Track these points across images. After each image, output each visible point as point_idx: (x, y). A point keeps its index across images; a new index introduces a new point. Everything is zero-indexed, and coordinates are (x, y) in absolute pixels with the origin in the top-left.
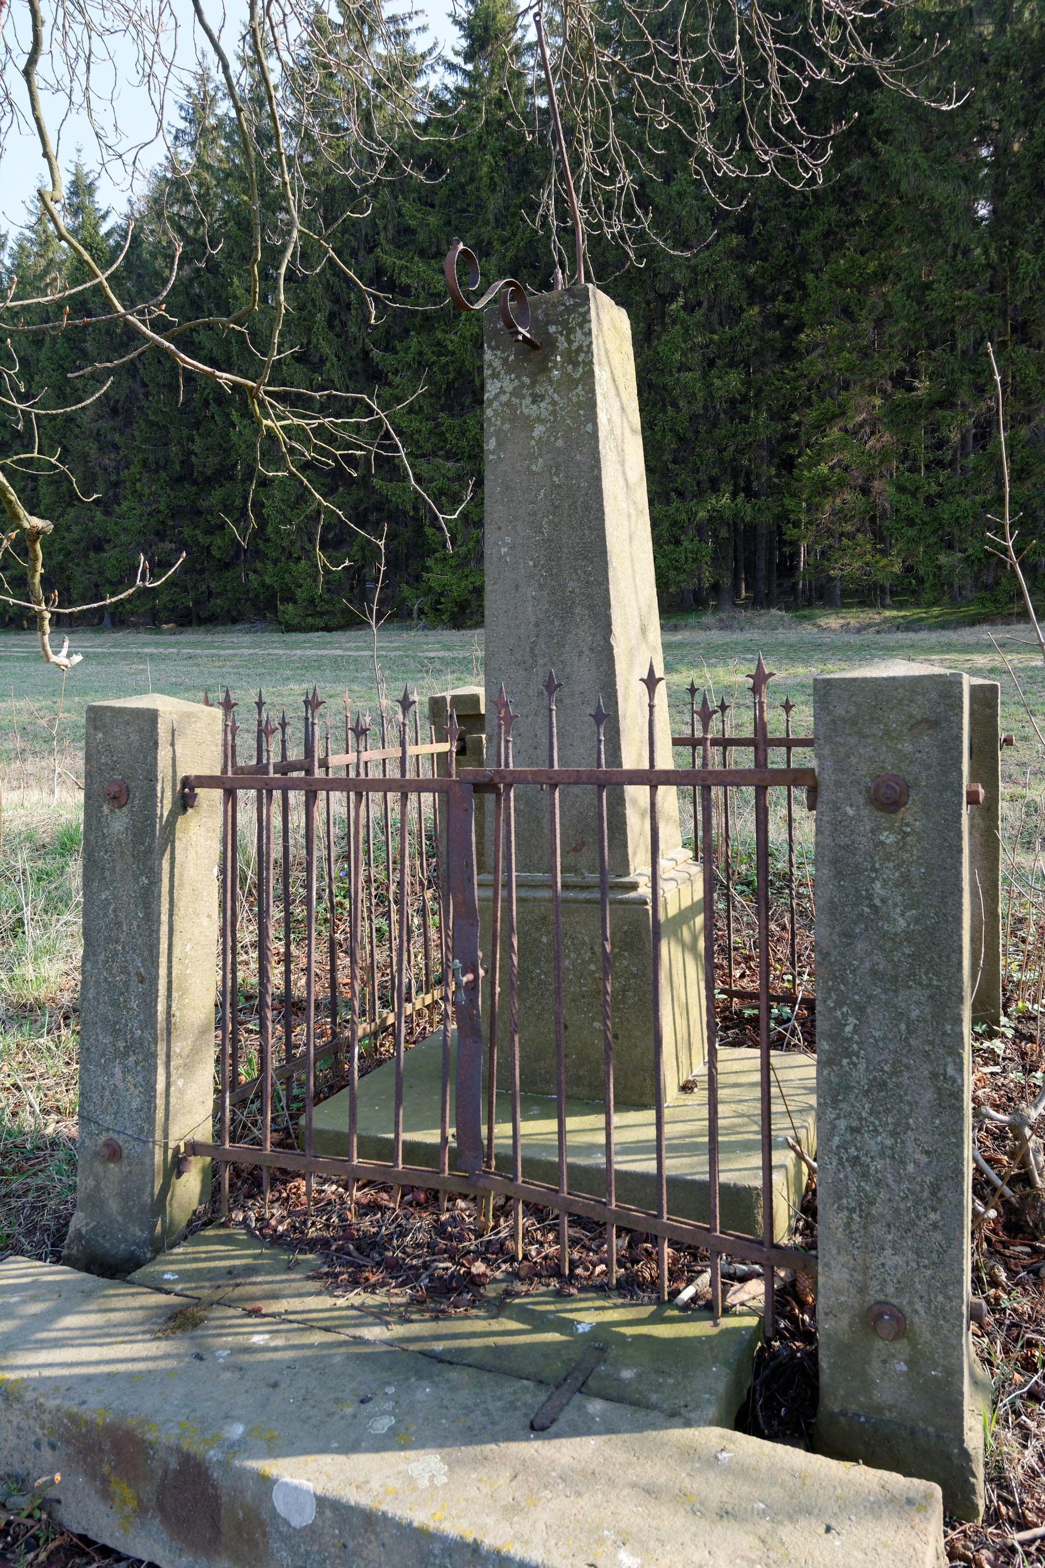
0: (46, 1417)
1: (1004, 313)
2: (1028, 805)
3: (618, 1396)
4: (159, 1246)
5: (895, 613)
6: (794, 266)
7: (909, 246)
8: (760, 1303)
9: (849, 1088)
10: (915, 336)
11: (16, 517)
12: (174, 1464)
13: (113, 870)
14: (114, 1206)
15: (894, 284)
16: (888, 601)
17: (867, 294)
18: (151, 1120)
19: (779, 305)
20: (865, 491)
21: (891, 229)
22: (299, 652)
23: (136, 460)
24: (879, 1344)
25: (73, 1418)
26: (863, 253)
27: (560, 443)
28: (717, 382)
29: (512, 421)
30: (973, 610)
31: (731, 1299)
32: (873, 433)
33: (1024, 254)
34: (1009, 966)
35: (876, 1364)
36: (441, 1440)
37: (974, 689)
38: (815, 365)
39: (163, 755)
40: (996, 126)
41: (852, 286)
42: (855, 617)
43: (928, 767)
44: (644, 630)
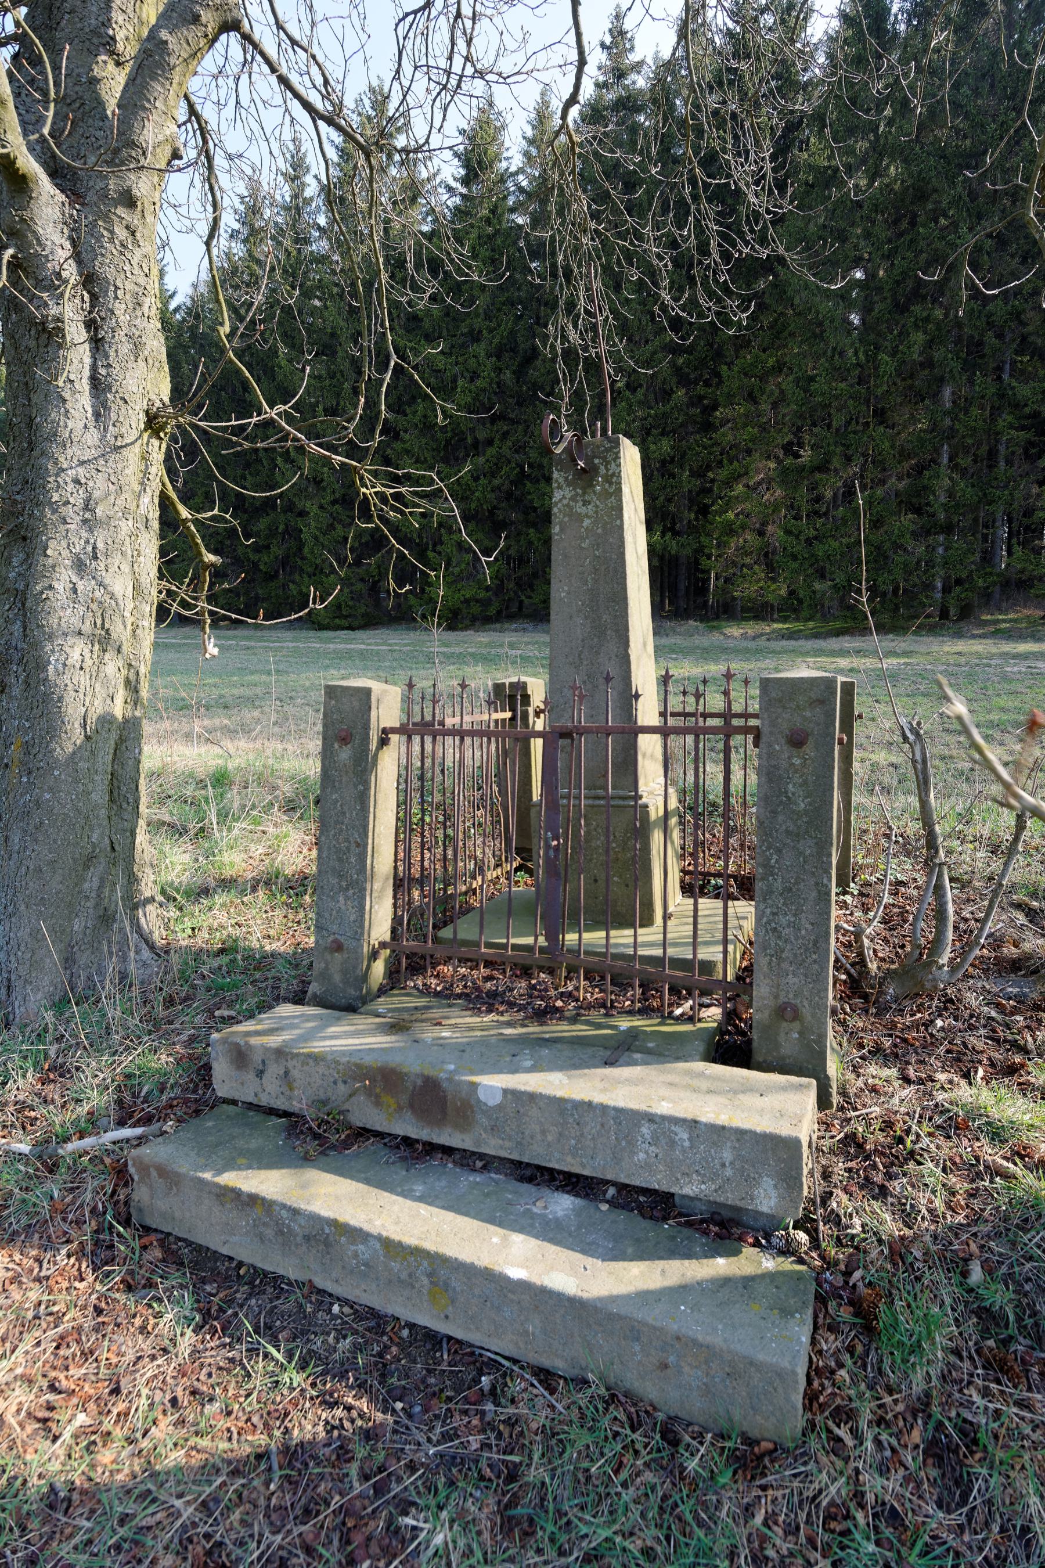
0: (340, 1067)
1: (867, 402)
2: (872, 765)
3: (649, 1052)
4: (365, 1000)
5: (781, 626)
6: (712, 359)
7: (799, 347)
8: (719, 1017)
9: (772, 892)
10: (801, 416)
11: (200, 554)
12: (419, 1082)
13: (340, 782)
14: (337, 978)
15: (787, 376)
16: (775, 616)
17: (766, 382)
18: (362, 927)
19: (701, 389)
20: (761, 533)
21: (786, 334)
22: (332, 646)
23: (199, 492)
24: (785, 1024)
25: (357, 1065)
26: (764, 351)
27: (600, 531)
28: (653, 447)
29: (570, 516)
30: (838, 624)
31: (702, 1015)
32: (768, 489)
33: (884, 357)
34: (858, 857)
35: (782, 1035)
36: (561, 1068)
37: (843, 684)
38: (726, 436)
39: (373, 714)
40: (866, 256)
41: (756, 376)
42: (751, 628)
43: (818, 724)
44: (645, 644)
